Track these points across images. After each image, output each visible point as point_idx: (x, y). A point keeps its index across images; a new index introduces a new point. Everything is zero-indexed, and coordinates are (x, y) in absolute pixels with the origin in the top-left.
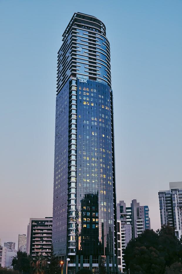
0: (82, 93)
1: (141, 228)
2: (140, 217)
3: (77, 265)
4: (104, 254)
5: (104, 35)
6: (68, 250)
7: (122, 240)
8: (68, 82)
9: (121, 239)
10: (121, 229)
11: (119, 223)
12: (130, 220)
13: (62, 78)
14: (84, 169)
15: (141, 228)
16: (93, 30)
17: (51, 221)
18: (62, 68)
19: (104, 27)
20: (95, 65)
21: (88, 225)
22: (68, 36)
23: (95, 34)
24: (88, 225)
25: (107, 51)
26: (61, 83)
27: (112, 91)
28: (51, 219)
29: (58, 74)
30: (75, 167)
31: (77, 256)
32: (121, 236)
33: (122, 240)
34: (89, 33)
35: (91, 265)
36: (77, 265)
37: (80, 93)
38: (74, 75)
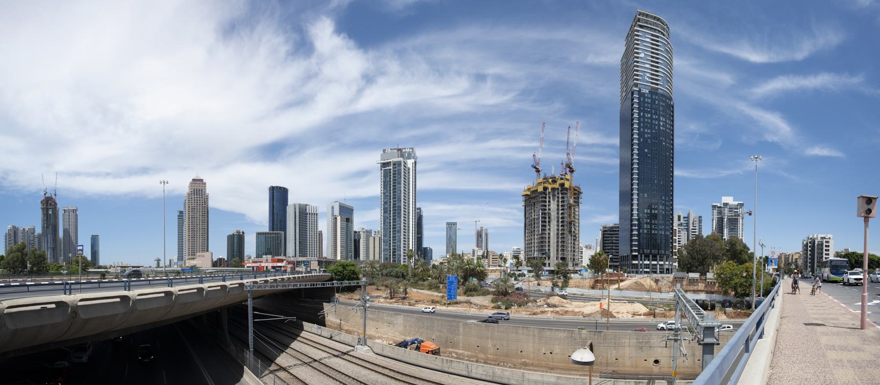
0: (644, 99)
1: (695, 232)
2: (695, 225)
3: (639, 262)
4: (664, 271)
5: (667, 38)
6: (632, 251)
7: (678, 244)
8: (630, 93)
9: (677, 243)
10: (677, 235)
11: (676, 230)
12: (686, 227)
13: (625, 89)
14: (166, 276)
15: (695, 232)
16: (656, 32)
17: (618, 227)
18: (625, 78)
19: (667, 29)
20: (657, 82)
21: (646, 116)
22: (631, 40)
23: (658, 37)
24: (646, 116)
25: (670, 58)
26: (624, 94)
27: (673, 103)
28: (618, 226)
29: (621, 84)
30: (863, 218)
31: (639, 256)
32: (677, 240)
33: (678, 244)
34: (653, 35)
35: (650, 263)
36: (639, 262)
37: (642, 120)
38: (636, 85)
